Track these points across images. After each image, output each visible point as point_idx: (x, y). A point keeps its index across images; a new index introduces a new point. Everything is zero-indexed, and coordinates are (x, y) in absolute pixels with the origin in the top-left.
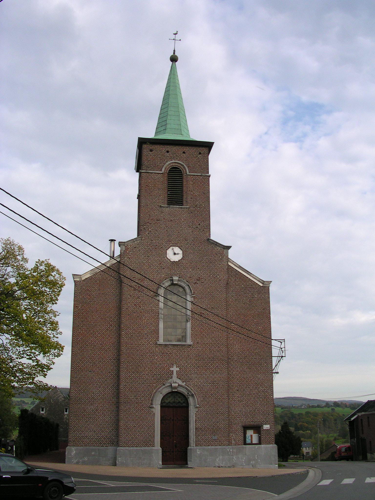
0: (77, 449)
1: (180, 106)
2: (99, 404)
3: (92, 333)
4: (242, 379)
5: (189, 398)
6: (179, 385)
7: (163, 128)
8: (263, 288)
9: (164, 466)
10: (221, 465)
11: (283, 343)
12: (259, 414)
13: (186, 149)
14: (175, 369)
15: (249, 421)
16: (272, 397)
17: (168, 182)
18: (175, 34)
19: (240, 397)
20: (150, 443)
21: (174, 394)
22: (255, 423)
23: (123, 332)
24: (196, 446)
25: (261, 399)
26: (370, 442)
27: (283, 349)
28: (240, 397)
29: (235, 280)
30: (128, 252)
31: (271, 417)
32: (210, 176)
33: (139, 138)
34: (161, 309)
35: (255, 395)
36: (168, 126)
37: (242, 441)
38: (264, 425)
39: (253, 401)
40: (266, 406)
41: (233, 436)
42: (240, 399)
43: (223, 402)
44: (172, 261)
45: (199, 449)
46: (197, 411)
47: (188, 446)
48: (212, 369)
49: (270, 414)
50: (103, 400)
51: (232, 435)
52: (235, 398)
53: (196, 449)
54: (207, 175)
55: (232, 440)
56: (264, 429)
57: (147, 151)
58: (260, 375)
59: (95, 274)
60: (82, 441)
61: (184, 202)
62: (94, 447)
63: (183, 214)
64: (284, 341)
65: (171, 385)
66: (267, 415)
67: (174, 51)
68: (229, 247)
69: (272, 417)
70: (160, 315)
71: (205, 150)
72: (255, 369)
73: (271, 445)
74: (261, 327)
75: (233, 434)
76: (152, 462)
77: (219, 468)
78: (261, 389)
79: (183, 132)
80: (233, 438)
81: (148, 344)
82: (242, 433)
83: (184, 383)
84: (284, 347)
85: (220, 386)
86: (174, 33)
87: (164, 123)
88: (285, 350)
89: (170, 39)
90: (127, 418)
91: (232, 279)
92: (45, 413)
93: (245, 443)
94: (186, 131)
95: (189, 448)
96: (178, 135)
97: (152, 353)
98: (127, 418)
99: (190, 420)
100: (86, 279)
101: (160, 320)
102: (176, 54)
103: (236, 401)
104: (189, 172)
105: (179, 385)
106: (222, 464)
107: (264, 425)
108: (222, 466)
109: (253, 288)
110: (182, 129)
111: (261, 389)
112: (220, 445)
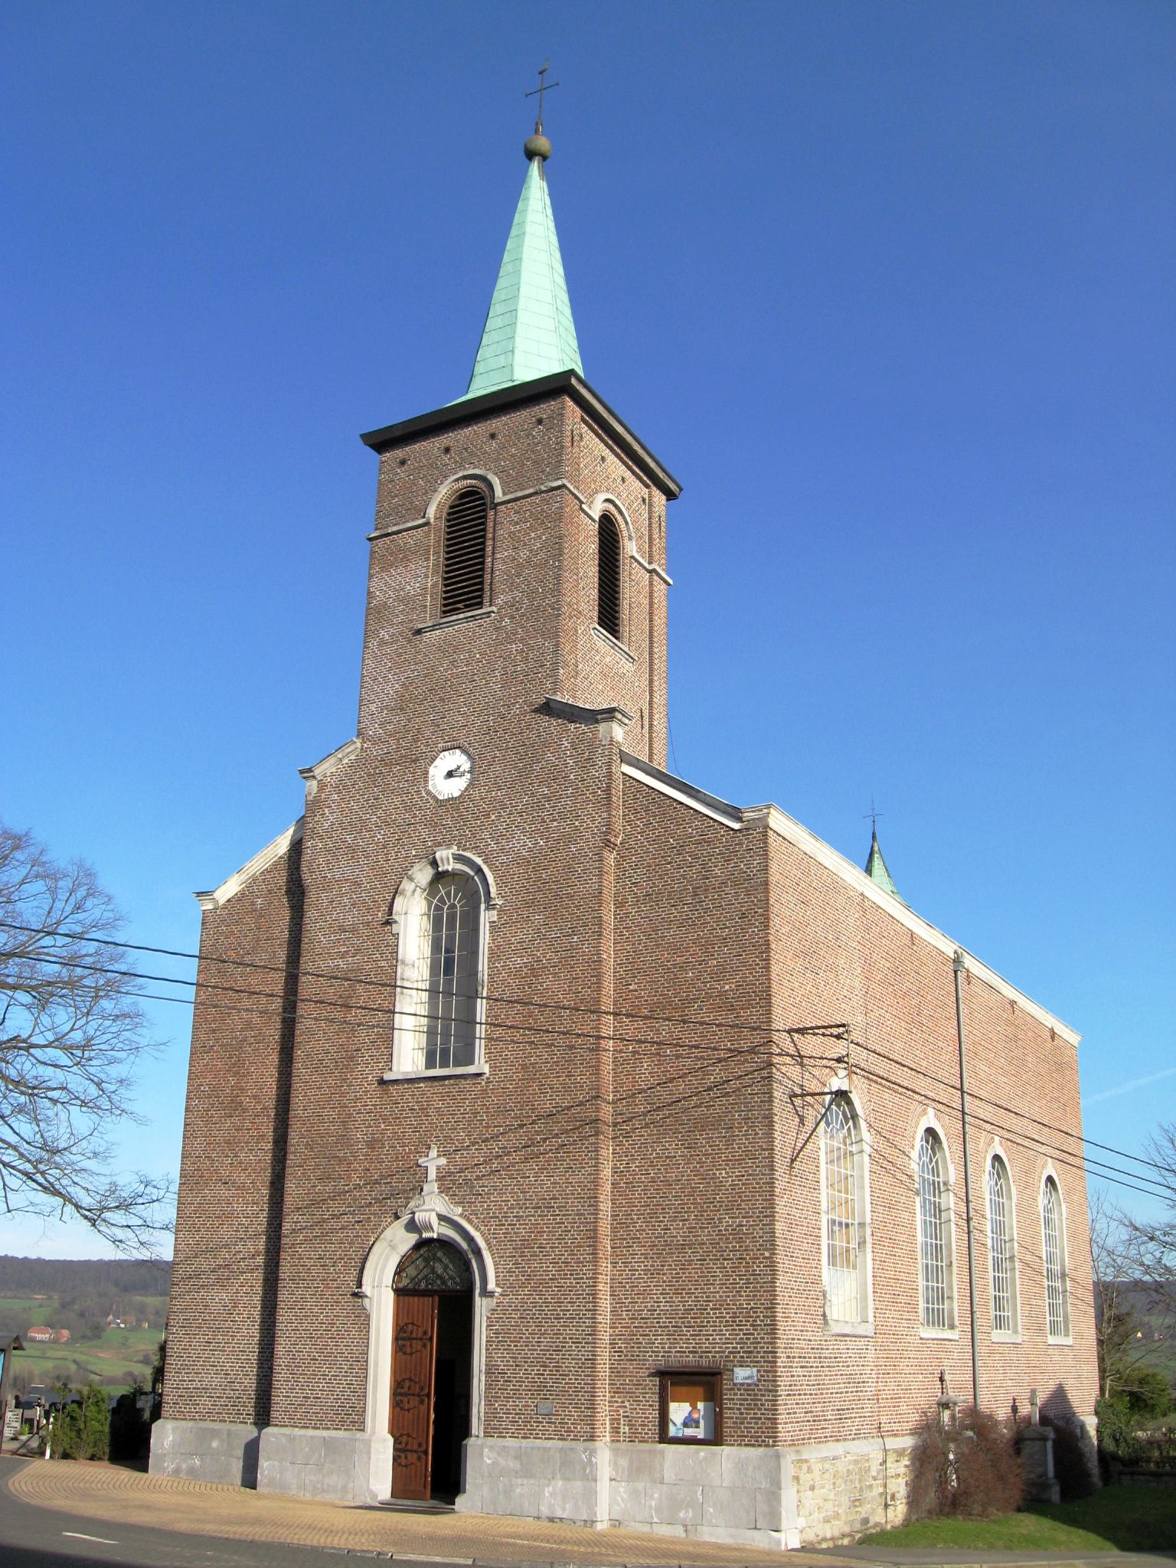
0: (177, 1427)
4: (662, 1189)
8: (743, 836)
9: (400, 1502)
10: (559, 1514)
12: (718, 1324)
14: (434, 1162)
15: (683, 1353)
16: (767, 1254)
19: (652, 1258)
20: (355, 1418)
22: (701, 1357)
23: (299, 1052)
24: (485, 1436)
25: (726, 1262)
28: (652, 1258)
30: (323, 795)
31: (765, 1334)
33: (361, 436)
35: (705, 1246)
37: (654, 1428)
38: (735, 1369)
39: (697, 1273)
40: (745, 1292)
41: (625, 1407)
42: (651, 1266)
43: (579, 1274)
44: (441, 798)
45: (491, 1448)
46: (493, 1310)
49: (759, 1323)
51: (620, 1400)
52: (636, 1262)
53: (482, 1447)
55: (622, 1422)
56: (735, 1384)
58: (725, 1169)
59: (250, 883)
61: (486, 600)
62: (212, 1425)
66: (748, 1327)
69: (768, 1334)
72: (708, 1148)
73: (762, 1449)
74: (733, 986)
75: (625, 1397)
76: (352, 1484)
77: (550, 1524)
78: (730, 1226)
80: (626, 1412)
85: (570, 1215)
89: (527, 96)
91: (638, 822)
93: (664, 1438)
100: (229, 901)
101: (397, 998)
103: (638, 1270)
106: (564, 1510)
107: (735, 1366)
108: (561, 1519)
111: (730, 1226)
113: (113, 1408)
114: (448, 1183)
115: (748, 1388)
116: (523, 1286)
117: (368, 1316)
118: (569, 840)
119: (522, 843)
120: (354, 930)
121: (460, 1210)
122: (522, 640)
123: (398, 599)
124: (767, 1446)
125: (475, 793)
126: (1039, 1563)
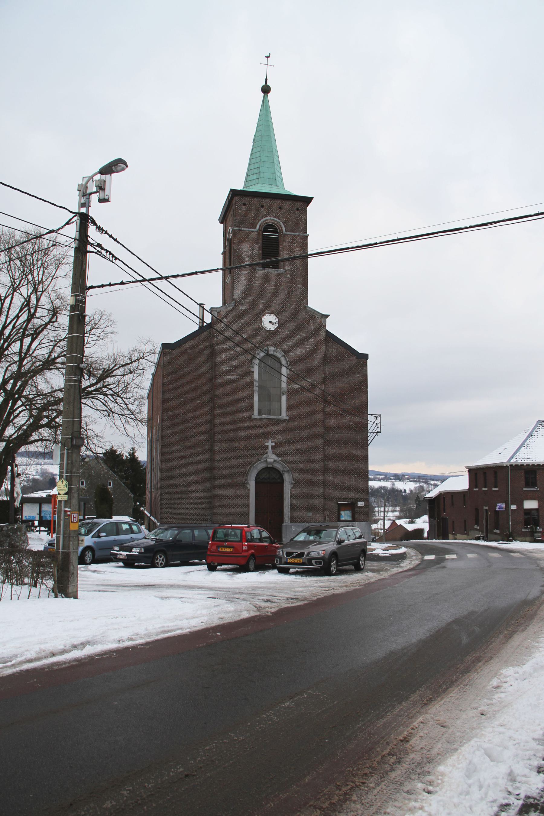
1: (274, 151)
2: (192, 480)
3: (183, 406)
5: (284, 474)
6: (275, 461)
7: (255, 177)
11: (379, 418)
13: (283, 203)
14: (270, 444)
17: (263, 242)
18: (268, 57)
21: (270, 470)
26: (453, 522)
27: (379, 425)
29: (333, 351)
32: (307, 236)
34: (255, 380)
36: (262, 175)
45: (294, 526)
47: (283, 522)
48: (307, 444)
50: (196, 476)
54: (305, 235)
57: (240, 205)
60: (175, 519)
63: (279, 278)
64: (380, 417)
65: (266, 460)
67: (266, 79)
68: (327, 316)
70: (255, 387)
71: (301, 205)
79: (278, 182)
81: (242, 418)
82: (336, 510)
83: (280, 459)
84: (380, 423)
86: (267, 55)
87: (256, 171)
88: (380, 426)
90: (222, 494)
92: (86, 487)
94: (280, 180)
95: (284, 524)
96: (273, 186)
97: (246, 427)
98: (222, 494)
99: (284, 496)
102: (268, 84)
104: (286, 231)
105: (275, 461)
109: (351, 360)
110: (277, 179)
112: (315, 522)
113: (115, 451)
114: (274, 451)
115: (361, 507)
116: (301, 481)
117: (249, 490)
118: (313, 352)
119: (298, 350)
120: (236, 367)
121: (280, 459)
122: (294, 284)
123: (246, 255)
124: (366, 521)
125: (280, 330)
126: (469, 541)
